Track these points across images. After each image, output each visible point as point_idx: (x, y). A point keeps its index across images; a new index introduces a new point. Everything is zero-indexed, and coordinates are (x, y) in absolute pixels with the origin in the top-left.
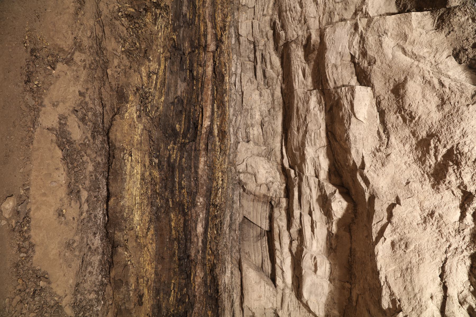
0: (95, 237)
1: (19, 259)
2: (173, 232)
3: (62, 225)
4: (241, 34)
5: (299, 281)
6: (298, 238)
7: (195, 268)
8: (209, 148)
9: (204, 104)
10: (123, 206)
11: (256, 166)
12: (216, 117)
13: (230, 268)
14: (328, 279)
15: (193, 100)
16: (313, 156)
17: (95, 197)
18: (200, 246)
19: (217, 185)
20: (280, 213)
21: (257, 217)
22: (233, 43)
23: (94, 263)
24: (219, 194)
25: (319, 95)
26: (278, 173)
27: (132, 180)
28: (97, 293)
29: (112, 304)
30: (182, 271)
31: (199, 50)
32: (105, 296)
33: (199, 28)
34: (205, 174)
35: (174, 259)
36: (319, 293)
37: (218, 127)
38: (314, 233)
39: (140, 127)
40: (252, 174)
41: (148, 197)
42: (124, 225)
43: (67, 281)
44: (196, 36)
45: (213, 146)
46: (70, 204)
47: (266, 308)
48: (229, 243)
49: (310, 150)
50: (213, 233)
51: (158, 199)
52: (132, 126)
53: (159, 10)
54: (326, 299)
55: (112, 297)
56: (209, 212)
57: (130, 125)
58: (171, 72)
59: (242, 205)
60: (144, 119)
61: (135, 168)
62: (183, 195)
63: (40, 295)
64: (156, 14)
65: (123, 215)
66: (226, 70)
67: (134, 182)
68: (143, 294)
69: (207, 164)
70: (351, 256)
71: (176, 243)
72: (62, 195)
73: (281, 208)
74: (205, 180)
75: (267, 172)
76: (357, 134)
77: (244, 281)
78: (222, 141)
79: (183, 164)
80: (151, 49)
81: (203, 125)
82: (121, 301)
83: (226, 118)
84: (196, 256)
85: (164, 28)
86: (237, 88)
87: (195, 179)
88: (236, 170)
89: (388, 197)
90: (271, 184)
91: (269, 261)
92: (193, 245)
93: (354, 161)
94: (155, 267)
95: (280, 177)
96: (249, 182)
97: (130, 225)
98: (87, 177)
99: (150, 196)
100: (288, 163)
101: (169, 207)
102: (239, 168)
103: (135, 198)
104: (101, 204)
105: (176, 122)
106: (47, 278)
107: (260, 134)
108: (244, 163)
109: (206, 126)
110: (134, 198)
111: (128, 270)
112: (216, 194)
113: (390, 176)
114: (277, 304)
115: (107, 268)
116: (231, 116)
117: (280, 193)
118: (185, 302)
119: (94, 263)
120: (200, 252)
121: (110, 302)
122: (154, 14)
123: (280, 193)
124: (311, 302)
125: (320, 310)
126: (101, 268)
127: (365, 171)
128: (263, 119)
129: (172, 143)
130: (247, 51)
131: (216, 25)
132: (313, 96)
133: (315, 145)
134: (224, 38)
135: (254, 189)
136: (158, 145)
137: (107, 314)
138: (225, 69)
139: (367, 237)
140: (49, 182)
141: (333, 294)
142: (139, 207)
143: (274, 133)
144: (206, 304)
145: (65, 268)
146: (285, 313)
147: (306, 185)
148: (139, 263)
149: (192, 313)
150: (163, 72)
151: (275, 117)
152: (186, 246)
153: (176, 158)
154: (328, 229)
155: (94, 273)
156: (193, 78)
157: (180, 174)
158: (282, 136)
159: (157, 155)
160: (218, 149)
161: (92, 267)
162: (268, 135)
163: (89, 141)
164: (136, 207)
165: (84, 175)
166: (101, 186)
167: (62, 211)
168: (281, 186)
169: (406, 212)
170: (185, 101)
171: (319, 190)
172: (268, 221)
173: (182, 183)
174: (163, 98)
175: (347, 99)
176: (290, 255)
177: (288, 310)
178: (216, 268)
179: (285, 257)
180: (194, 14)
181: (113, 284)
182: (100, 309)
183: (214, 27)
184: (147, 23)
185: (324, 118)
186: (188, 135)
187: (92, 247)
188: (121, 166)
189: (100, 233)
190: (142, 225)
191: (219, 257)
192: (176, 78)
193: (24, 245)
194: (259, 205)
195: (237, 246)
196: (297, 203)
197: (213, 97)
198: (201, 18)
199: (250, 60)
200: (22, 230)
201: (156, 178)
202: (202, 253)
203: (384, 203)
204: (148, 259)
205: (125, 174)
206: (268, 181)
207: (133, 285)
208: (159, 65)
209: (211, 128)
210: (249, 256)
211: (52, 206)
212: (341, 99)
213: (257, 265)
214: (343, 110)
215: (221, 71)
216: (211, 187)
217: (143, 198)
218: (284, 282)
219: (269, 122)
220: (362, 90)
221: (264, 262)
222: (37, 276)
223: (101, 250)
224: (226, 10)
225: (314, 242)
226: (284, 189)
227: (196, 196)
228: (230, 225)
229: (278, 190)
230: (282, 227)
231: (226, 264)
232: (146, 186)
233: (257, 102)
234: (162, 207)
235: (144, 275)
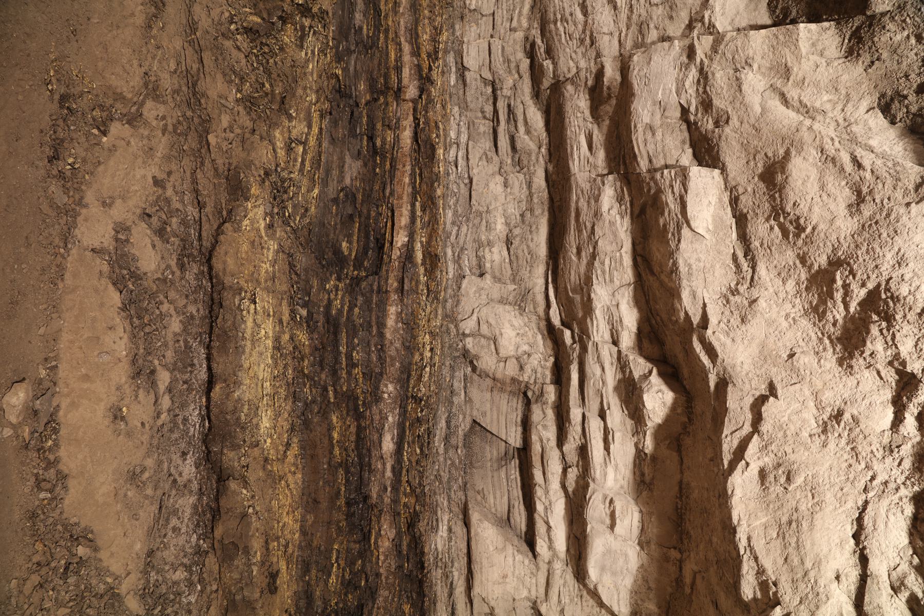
0: (185, 460)
1: (37, 503)
2: (337, 451)
4: (468, 66)
5: (579, 546)
6: (578, 462)
7: (379, 522)
8: (406, 288)
9: (395, 202)
11: (497, 322)
13: (446, 520)
14: (637, 541)
15: (375, 195)
16: (608, 303)
17: (185, 382)
18: (389, 478)
19: (422, 359)
20: (544, 413)
22: (452, 84)
24: (426, 378)
25: (618, 184)
26: (539, 337)
27: (257, 349)
28: (188, 568)
29: (217, 590)
31: (386, 98)
32: (205, 575)
33: (387, 54)
34: (399, 339)
35: (338, 503)
37: (422, 246)
38: (609, 454)
39: (271, 247)
40: (488, 339)
44: (380, 70)
45: (414, 283)
46: (137, 397)
47: (517, 598)
48: (444, 472)
50: (414, 453)
51: (308, 386)
52: (256, 244)
53: (309, 20)
54: (632, 580)
55: (218, 577)
56: (405, 412)
57: (253, 243)
58: (333, 141)
59: (470, 399)
61: (263, 326)
62: (356, 379)
63: (77, 573)
64: (303, 28)
65: (238, 419)
66: (438, 136)
68: (278, 572)
69: (402, 319)
71: (341, 471)
75: (518, 334)
78: (430, 275)
79: (355, 318)
80: (294, 95)
81: (394, 243)
82: (235, 584)
84: (380, 497)
85: (318, 54)
86: (459, 171)
87: (379, 347)
88: (457, 330)
91: (522, 507)
92: (375, 476)
93: (686, 313)
96: (482, 354)
97: (253, 436)
98: (170, 343)
99: (290, 380)
101: (329, 401)
102: (464, 327)
103: (262, 385)
105: (341, 237)
106: (91, 541)
107: (504, 259)
108: (475, 317)
109: (399, 244)
110: (260, 385)
111: (249, 524)
112: (421, 376)
113: (758, 340)
114: (537, 591)
115: (208, 520)
116: (448, 226)
117: (544, 375)
120: (389, 489)
121: (215, 587)
122: (298, 28)
123: (544, 375)
125: (621, 602)
129: (333, 277)
130: (480, 99)
131: (418, 48)
132: (607, 187)
133: (612, 281)
134: (434, 74)
135: (493, 367)
136: (307, 281)
137: (208, 609)
138: (437, 135)
139: (711, 460)
140: (96, 353)
141: (646, 571)
142: (270, 402)
144: (401, 591)
145: (126, 521)
146: (554, 608)
147: (593, 359)
148: (269, 510)
149: (373, 607)
150: (317, 139)
151: (534, 227)
152: (361, 477)
153: (342, 306)
154: (636, 445)
156: (374, 151)
158: (548, 264)
159: (305, 301)
160: (422, 290)
161: (179, 519)
163: (173, 273)
165: (162, 340)
166: (196, 361)
167: (121, 410)
168: (546, 361)
169: (789, 411)
170: (360, 197)
171: (619, 369)
172: (520, 429)
173: (354, 355)
174: (316, 191)
175: (673, 192)
177: (560, 602)
178: (419, 521)
179: (553, 499)
180: (377, 27)
181: (219, 552)
182: (193, 601)
183: (416, 53)
184: (286, 44)
186: (365, 263)
187: (179, 479)
188: (234, 323)
189: (193, 453)
190: (275, 437)
191: (424, 500)
192: (342, 152)
193: (47, 475)
194: (502, 397)
197: (414, 188)
198: (391, 35)
199: (485, 117)
200: (43, 447)
201: (304, 345)
203: (745, 395)
204: (287, 503)
205: (244, 338)
206: (520, 351)
207: (259, 553)
208: (310, 127)
209: (409, 249)
213: (499, 516)
215: (429, 138)
216: (410, 364)
217: (277, 384)
218: (551, 547)
221: (511, 509)
222: (71, 536)
223: (196, 486)
224: (439, 19)
225: (610, 471)
227: (380, 381)
229: (539, 370)
231: (439, 512)
232: (284, 362)
233: (499, 198)
235: (280, 534)
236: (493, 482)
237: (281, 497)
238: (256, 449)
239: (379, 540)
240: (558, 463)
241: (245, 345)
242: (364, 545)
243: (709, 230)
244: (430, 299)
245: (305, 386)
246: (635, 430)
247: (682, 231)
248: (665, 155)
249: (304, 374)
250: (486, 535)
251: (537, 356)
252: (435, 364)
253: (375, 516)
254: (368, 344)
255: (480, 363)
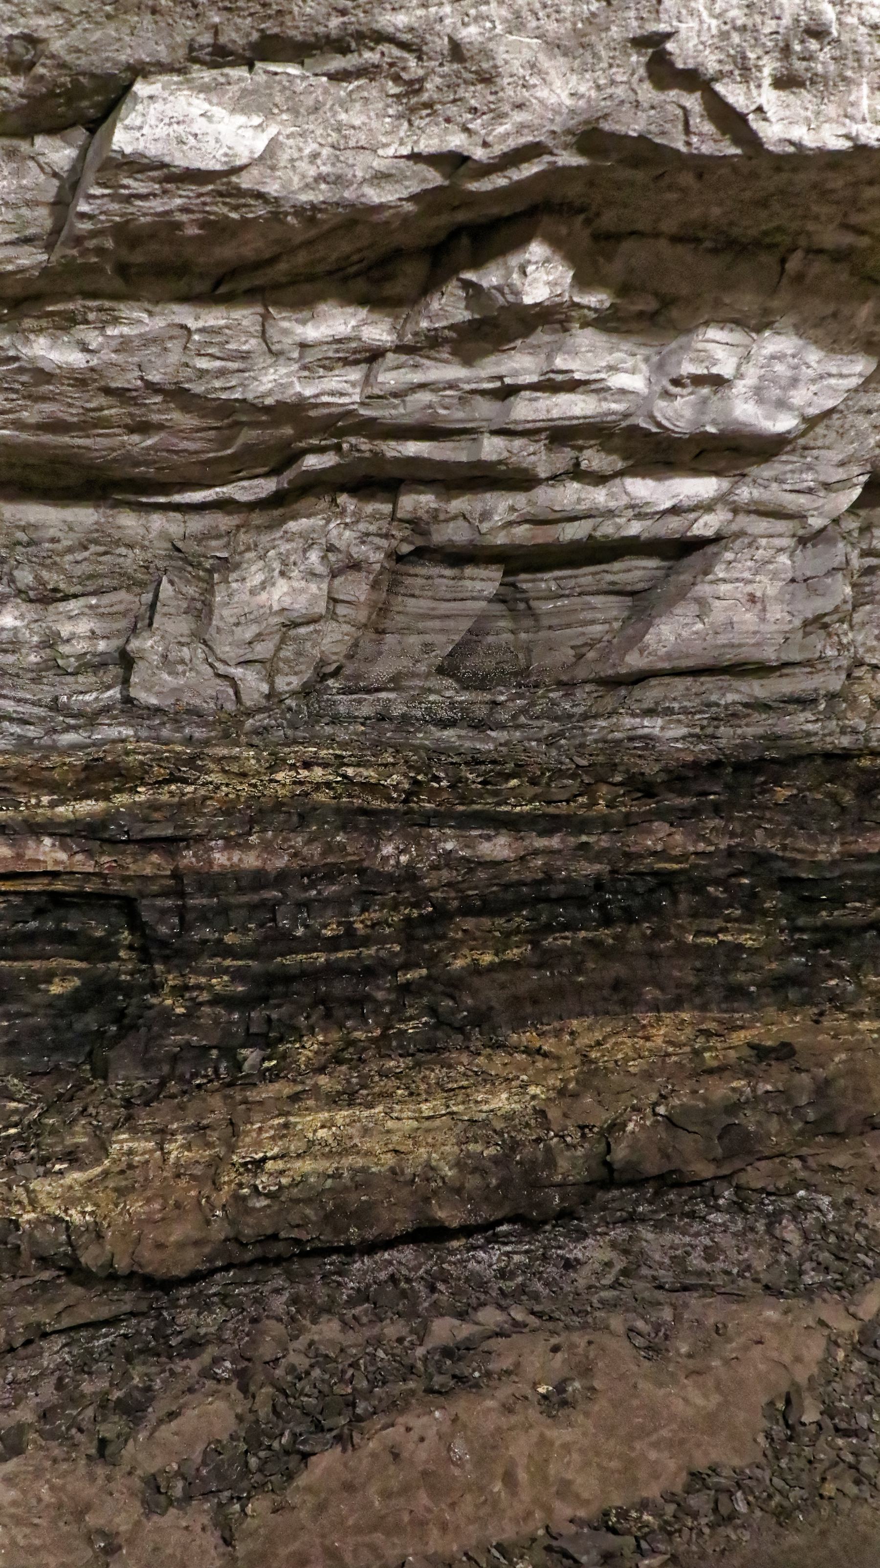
0: (577, 1260)
1: (758, 1513)
2: (513, 954)
3: (597, 1384)
5: (715, 450)
6: (573, 447)
7: (641, 856)
8: (169, 832)
10: (459, 1164)
11: (255, 621)
12: (11, 813)
13: (632, 721)
14: (754, 335)
16: (295, 367)
17: (433, 1289)
18: (562, 841)
19: (328, 785)
20: (455, 518)
21: (448, 617)
23: (671, 1248)
24: (370, 774)
25: (28, 323)
26: (293, 526)
27: (356, 1141)
28: (774, 1219)
29: (801, 1158)
30: (652, 910)
32: (781, 1185)
34: (285, 840)
35: (611, 941)
36: (789, 373)
37: (62, 802)
38: (586, 382)
40: (283, 641)
41: (413, 1068)
42: (528, 1150)
43: (776, 1327)
45: (157, 816)
46: (508, 1373)
47: (790, 575)
48: (542, 728)
49: (265, 379)
50: (518, 791)
51: (403, 1026)
52: (124, 1183)
54: (813, 348)
55: (777, 1160)
56: (436, 814)
59: (392, 679)
60: (73, 1135)
61: (310, 1135)
62: (373, 926)
63: (849, 1414)
65: (495, 1160)
67: (366, 1131)
68: (751, 1046)
69: (239, 835)
70: (698, 240)
71: (548, 942)
72: (489, 1410)
73: (435, 515)
74: (309, 842)
75: (282, 574)
76: (312, 172)
77: (690, 663)
78: (134, 778)
79: (249, 938)
81: (60, 868)
82: (788, 1122)
83: (18, 768)
84: (599, 856)
87: (306, 880)
88: (260, 710)
89: (619, 78)
90: (332, 557)
91: (617, 566)
92: (559, 870)
93: (408, 199)
94: (651, 1010)
95: (308, 516)
96: (316, 652)
97: (527, 1125)
98: (368, 1334)
99: (409, 1061)
100: (256, 482)
101: (429, 977)
102: (256, 696)
103: (428, 1118)
104: (450, 1263)
105: (37, 998)
106: (788, 1402)
107: (91, 607)
108: (237, 672)
109: (63, 856)
110: (427, 1124)
111: (686, 1110)
112: (368, 787)
113: (541, 57)
114: (780, 535)
115: (680, 1195)
117: (374, 517)
118: (752, 886)
119: (671, 1248)
120: (584, 838)
121: (796, 1164)
123: (374, 517)
124: (810, 405)
125: (845, 371)
126: (681, 1219)
127: (479, 154)
128: (19, 592)
129: (155, 1001)
132: (26, 351)
133: (245, 356)
135: (346, 628)
136: (174, 1059)
137: (836, 1169)
139: (700, 176)
140: (457, 1472)
141: (805, 321)
142: (460, 1098)
143: (96, 542)
144: (752, 807)
145: (734, 1344)
146: (820, 502)
147: (395, 407)
148: (648, 1075)
149: (783, 859)
151: (21, 536)
152: (560, 900)
153: (226, 971)
154: (585, 324)
155: (707, 1242)
157: (292, 944)
158: (118, 504)
161: (688, 1254)
162: (101, 569)
163: (217, 1361)
164: (461, 1108)
165: (370, 1349)
166: (383, 1275)
167: (545, 1397)
168: (343, 513)
169: (705, 15)
171: (433, 353)
172: (469, 571)
173: (329, 933)
175: (144, 197)
176: (617, 481)
177: (810, 491)
178: (643, 774)
179: (624, 500)
181: (738, 1164)
182: (826, 1200)
185: (150, 307)
186: (99, 934)
187: (619, 1266)
188: (308, 1201)
189: (560, 1248)
190: (525, 1078)
191: (601, 765)
193: (708, 1507)
194: (400, 609)
195: (551, 695)
196: (450, 445)
200: (662, 1529)
201: (325, 1044)
202: (589, 834)
203: (632, 97)
204: (629, 1042)
205: (337, 1175)
206: (320, 569)
207: (734, 1084)
210: (591, 646)
211: (542, 1435)
212: (127, 222)
213: (626, 614)
214: (184, 218)
216: (338, 811)
217: (423, 1087)
218: (707, 507)
219: (43, 565)
220: (138, 123)
221: (617, 588)
222: (790, 1439)
223: (618, 1231)
225: (619, 381)
226: (360, 500)
227: (379, 874)
228: (475, 727)
229: (362, 526)
230: (516, 510)
231: (618, 735)
232: (377, 1078)
234: (432, 1011)
235: (687, 1049)
236: (562, 627)
237: (620, 1056)
238: (550, 1115)
239: (673, 853)
240: (562, 489)
241: (351, 1168)
242: (681, 883)
243: (260, 125)
244: (191, 774)
245: (402, 1032)
246: (557, 326)
247: (244, 186)
248: (28, 204)
249: (384, 1035)
250: (672, 638)
251: (335, 532)
252: (337, 757)
253: (627, 865)
254: (306, 904)
255: (334, 658)
